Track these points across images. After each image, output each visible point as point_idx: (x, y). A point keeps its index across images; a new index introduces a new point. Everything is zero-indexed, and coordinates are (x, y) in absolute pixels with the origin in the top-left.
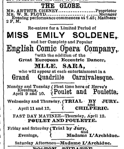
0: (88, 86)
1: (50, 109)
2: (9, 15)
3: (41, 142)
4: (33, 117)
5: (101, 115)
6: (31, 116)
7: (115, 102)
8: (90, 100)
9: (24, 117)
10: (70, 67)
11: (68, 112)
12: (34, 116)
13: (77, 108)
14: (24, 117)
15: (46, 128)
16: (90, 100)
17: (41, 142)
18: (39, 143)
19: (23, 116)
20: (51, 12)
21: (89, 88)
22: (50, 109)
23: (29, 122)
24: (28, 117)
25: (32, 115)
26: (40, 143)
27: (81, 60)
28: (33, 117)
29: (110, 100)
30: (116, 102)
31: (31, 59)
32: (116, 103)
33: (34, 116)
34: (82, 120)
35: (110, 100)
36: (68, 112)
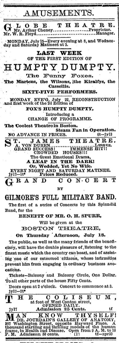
0: (57, 204)
1: (91, 303)
2: (7, 35)
3: (61, 235)
4: (26, 101)
5: (100, 234)
6: (79, 171)
7: (90, 109)
8: (58, 188)
9: (60, 60)
10: (43, 163)
11: (50, 38)
12: (25, 42)
13: (29, 119)
14: (60, 60)
15: (80, 323)
16: (58, 188)
17: (61, 235)
18: (59, 235)
19: (59, 59)
20: (109, 199)
21: (57, 206)
22: (91, 303)
23: (27, 110)
24: (76, 158)
25: (26, 99)
26: (60, 236)
27: (46, 174)
28: (26, 101)
29: (93, 215)
30: (92, 109)
31: (31, 125)
32: (92, 110)
33: (27, 100)
34: (37, 161)
35: (93, 215)
36: (50, 38)
